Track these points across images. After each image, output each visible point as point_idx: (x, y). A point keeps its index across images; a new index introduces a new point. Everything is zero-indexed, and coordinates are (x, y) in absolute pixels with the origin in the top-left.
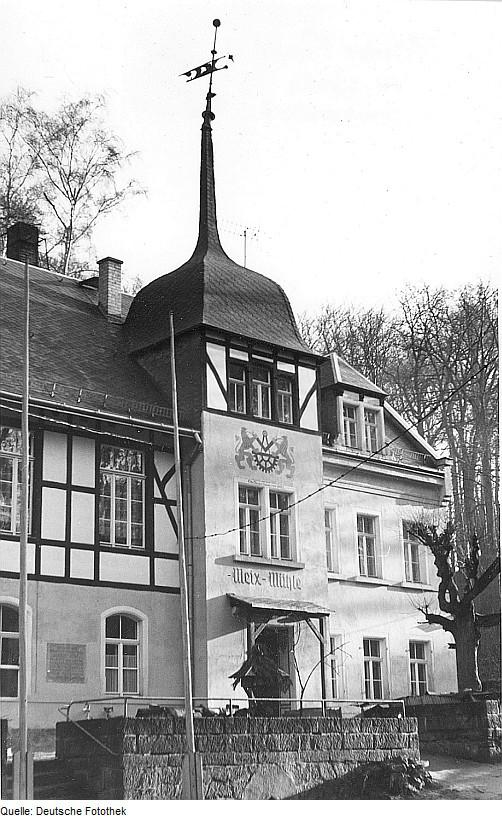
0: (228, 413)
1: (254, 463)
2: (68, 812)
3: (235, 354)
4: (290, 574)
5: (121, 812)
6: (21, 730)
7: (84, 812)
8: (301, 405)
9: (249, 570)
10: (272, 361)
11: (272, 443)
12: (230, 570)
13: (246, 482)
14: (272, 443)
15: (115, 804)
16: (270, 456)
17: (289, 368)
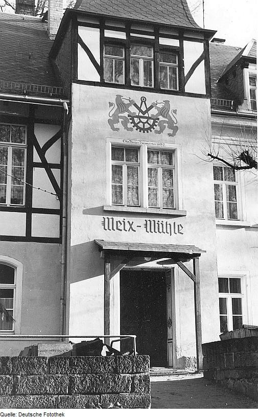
0: (102, 84)
1: (130, 125)
2: (35, 415)
3: (109, 34)
4: (171, 221)
5: (62, 415)
6: (120, 337)
7: (43, 415)
8: (186, 73)
9: (121, 219)
10: (153, 38)
11: (151, 107)
12: (100, 218)
13: (120, 141)
14: (151, 107)
15: (59, 411)
16: (148, 118)
17: (175, 43)
